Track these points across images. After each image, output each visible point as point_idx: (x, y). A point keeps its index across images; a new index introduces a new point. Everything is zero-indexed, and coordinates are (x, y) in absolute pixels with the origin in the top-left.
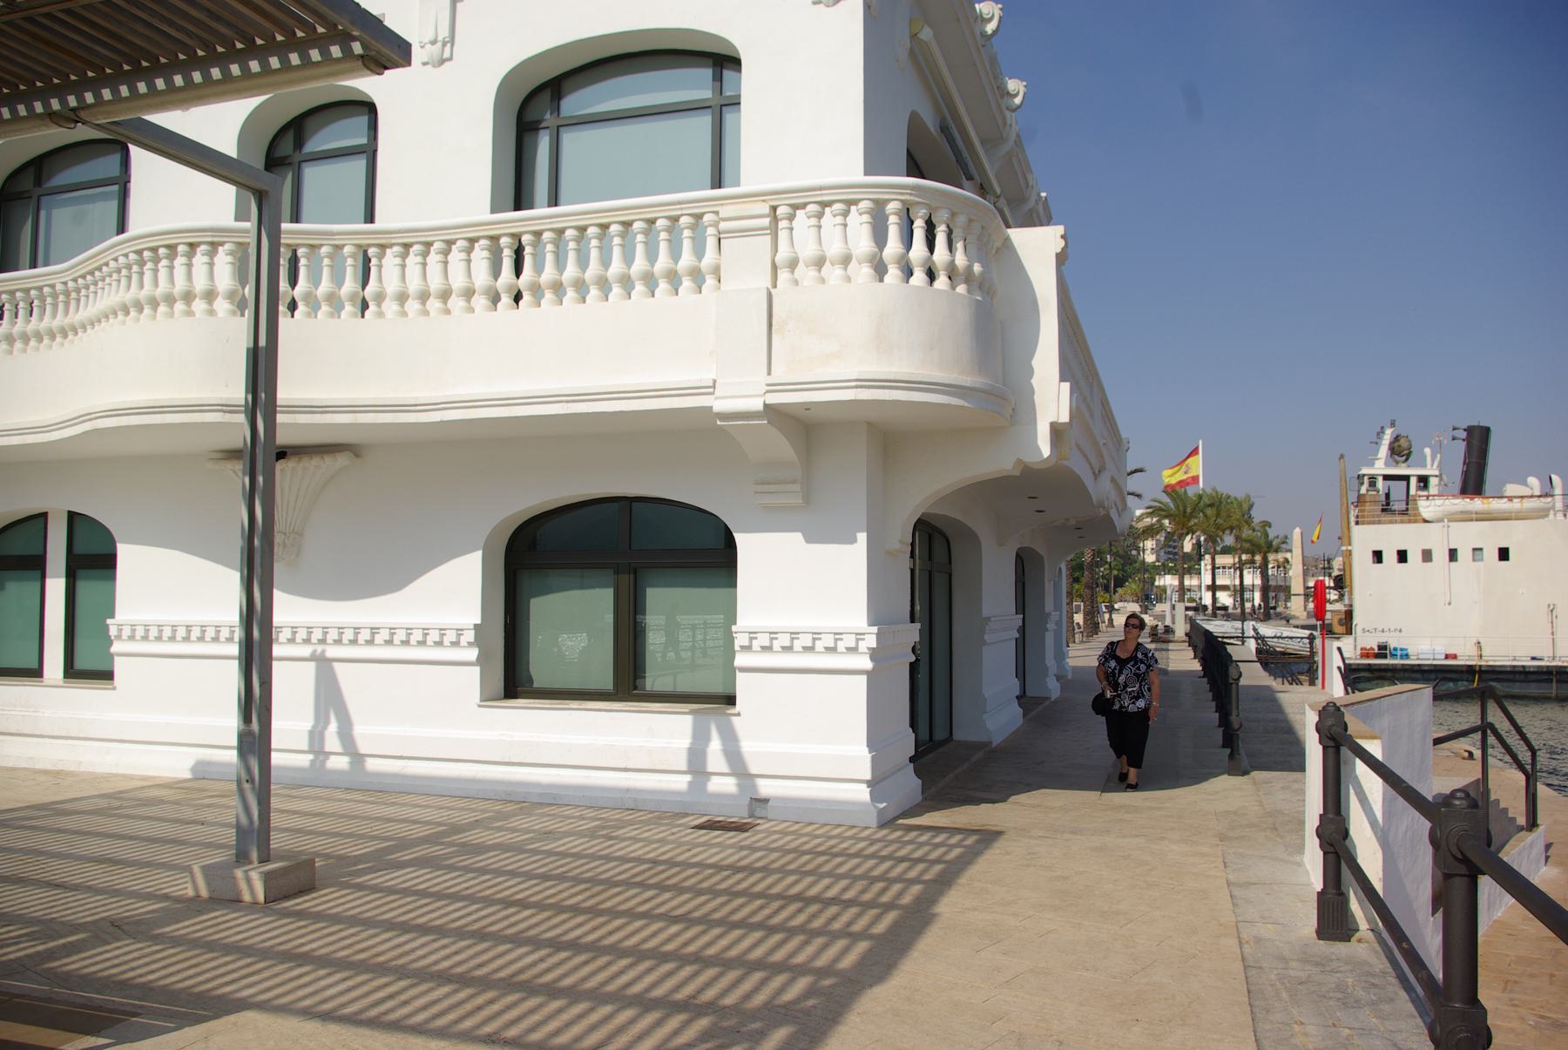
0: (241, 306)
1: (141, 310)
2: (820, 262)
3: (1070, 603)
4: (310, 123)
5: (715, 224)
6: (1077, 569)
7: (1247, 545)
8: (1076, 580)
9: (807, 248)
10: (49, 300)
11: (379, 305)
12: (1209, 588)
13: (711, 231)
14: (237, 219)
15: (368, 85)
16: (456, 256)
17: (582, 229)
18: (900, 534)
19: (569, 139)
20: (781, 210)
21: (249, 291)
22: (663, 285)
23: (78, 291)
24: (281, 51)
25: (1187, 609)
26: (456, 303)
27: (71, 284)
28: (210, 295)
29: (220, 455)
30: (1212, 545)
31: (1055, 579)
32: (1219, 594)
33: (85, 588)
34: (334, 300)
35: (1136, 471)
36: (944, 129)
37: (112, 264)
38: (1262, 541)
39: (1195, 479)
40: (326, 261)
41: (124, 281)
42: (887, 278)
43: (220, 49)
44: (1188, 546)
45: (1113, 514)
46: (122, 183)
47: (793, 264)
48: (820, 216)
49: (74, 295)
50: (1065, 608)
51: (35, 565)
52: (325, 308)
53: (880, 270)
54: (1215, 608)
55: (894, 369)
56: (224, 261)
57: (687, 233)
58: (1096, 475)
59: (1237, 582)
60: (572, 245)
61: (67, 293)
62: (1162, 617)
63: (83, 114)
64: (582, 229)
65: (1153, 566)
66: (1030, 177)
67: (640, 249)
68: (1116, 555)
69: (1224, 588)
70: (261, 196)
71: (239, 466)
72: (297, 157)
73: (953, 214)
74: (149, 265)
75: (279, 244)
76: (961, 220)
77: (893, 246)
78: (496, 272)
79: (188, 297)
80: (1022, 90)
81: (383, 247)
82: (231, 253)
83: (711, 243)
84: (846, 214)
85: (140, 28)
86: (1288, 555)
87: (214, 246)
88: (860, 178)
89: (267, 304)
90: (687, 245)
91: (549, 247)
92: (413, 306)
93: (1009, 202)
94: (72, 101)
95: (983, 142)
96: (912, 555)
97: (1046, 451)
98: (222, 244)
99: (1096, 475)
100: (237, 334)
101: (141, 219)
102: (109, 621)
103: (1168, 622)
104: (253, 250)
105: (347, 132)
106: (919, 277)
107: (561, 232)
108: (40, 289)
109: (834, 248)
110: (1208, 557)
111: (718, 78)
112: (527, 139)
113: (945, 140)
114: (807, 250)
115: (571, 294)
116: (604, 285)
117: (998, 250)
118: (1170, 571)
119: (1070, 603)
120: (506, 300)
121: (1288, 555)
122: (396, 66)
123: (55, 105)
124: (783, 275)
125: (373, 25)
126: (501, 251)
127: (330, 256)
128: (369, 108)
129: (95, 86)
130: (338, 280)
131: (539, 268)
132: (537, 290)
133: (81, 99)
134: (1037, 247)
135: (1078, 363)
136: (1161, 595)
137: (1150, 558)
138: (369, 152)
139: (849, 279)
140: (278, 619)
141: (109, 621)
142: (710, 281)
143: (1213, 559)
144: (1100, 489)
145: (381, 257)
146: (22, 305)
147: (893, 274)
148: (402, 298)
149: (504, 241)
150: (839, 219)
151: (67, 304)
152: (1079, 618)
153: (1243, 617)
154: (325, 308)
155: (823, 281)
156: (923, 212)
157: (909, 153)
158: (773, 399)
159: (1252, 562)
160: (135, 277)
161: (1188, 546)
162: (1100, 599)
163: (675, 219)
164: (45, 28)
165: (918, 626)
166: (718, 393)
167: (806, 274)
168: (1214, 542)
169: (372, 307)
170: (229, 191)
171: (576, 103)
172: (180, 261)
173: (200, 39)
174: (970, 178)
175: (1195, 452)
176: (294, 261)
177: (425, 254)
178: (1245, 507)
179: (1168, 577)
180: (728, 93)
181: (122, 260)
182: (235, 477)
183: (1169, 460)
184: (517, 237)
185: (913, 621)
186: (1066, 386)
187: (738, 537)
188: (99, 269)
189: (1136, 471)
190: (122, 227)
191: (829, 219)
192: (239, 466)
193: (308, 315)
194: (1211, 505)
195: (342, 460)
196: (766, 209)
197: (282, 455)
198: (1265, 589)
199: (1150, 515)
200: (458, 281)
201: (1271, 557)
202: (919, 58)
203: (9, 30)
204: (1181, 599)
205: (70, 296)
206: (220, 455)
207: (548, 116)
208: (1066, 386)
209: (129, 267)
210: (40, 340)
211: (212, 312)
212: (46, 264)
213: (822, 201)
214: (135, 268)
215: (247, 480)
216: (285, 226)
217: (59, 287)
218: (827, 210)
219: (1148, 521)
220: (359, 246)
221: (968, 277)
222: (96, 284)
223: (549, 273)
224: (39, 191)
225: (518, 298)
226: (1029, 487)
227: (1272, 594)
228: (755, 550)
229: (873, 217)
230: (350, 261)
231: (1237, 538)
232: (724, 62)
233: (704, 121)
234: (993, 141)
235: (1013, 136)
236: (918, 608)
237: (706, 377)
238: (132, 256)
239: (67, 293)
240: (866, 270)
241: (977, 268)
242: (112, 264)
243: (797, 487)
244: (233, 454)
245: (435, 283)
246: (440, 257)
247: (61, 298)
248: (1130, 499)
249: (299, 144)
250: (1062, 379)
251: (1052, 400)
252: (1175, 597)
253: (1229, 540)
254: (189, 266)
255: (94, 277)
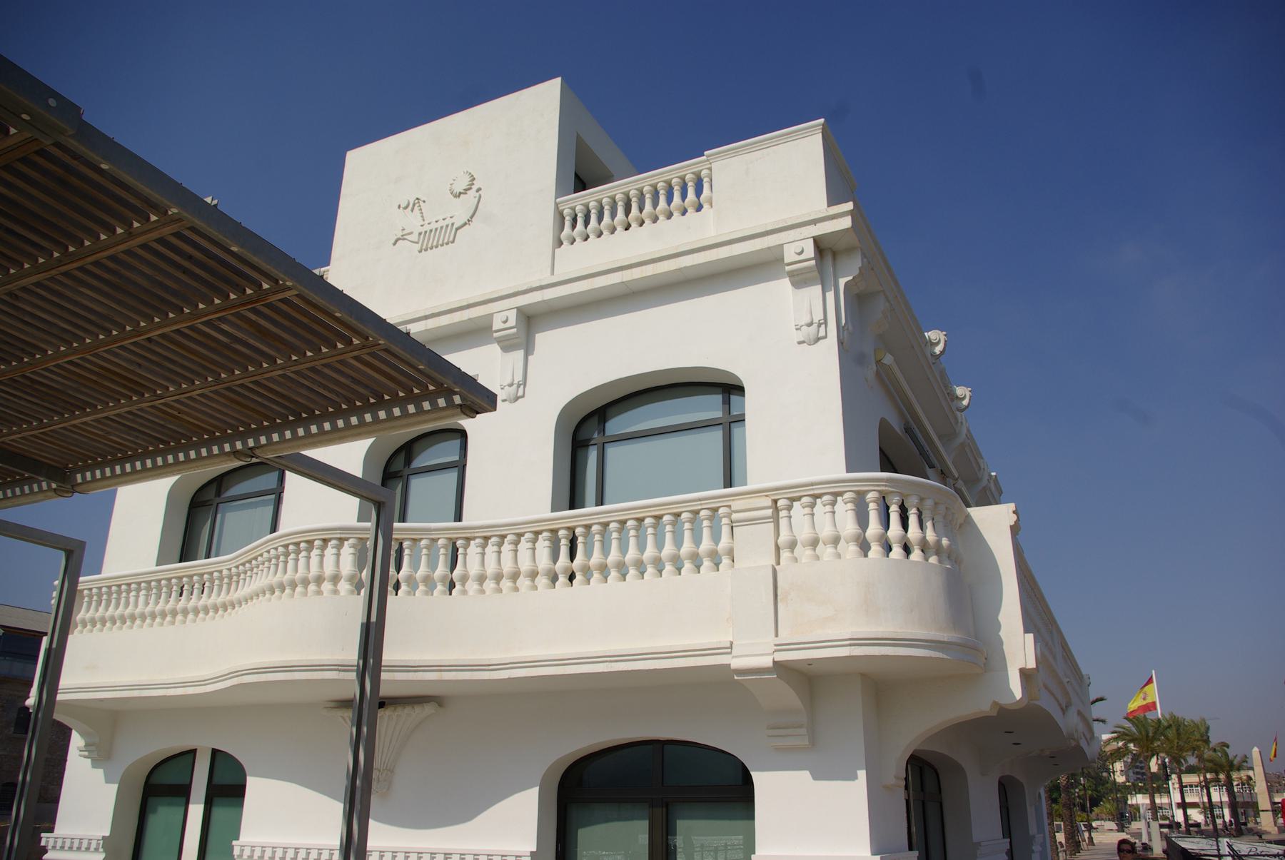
0: (358, 586)
1: (283, 590)
2: (814, 543)
3: (1051, 824)
4: (417, 446)
5: (728, 516)
6: (1054, 790)
7: (1209, 765)
8: (1055, 801)
9: (803, 532)
10: (217, 582)
11: (463, 585)
12: (1179, 805)
13: (725, 521)
14: (359, 521)
15: (466, 423)
16: (524, 545)
17: (623, 522)
18: (895, 770)
19: (612, 452)
20: (780, 503)
21: (365, 574)
22: (688, 565)
23: (238, 575)
24: (402, 403)
25: (1162, 826)
26: (524, 582)
27: (234, 570)
28: (335, 579)
29: (332, 704)
30: (1177, 765)
31: (1036, 801)
32: (1189, 811)
33: (219, 813)
34: (428, 580)
35: (1097, 700)
36: (908, 430)
37: (266, 555)
38: (1224, 760)
39: (1152, 706)
40: (425, 551)
41: (273, 567)
42: (871, 554)
43: (358, 404)
44: (1154, 766)
45: (1083, 744)
46: (278, 494)
47: (792, 545)
48: (813, 506)
49: (235, 578)
50: (1047, 828)
51: (182, 793)
52: (422, 587)
53: (864, 547)
54: (1188, 825)
55: (881, 629)
56: (348, 552)
57: (706, 523)
58: (1064, 711)
59: (1206, 799)
60: (615, 535)
61: (230, 577)
62: (1139, 835)
63: (257, 452)
64: (623, 522)
65: (1123, 786)
66: (980, 461)
67: (668, 537)
68: (1087, 776)
69: (1194, 805)
70: (379, 506)
71: (349, 714)
72: (406, 471)
73: (922, 500)
74: (292, 556)
75: (391, 539)
76: (929, 503)
77: (874, 527)
78: (555, 557)
79: (319, 580)
80: (943, 339)
81: (468, 539)
82: (353, 546)
83: (725, 530)
84: (833, 503)
85: (304, 392)
86: (1250, 773)
87: (342, 540)
88: (843, 474)
89: (379, 584)
90: (706, 533)
91: (597, 537)
92: (489, 585)
93: (965, 482)
94: (251, 443)
95: (940, 437)
96: (907, 787)
97: (1018, 694)
98: (347, 539)
99: (1064, 711)
100: (354, 609)
101: (290, 521)
102: (234, 843)
103: (1145, 839)
104: (370, 544)
105: (444, 452)
106: (897, 552)
107: (606, 525)
108: (211, 574)
109: (826, 531)
110: (1174, 776)
111: (727, 402)
112: (580, 453)
113: (910, 442)
114: (804, 533)
115: (614, 574)
116: (640, 567)
117: (961, 526)
118: (1140, 790)
119: (1051, 824)
120: (562, 579)
121: (1250, 773)
122: (486, 411)
123: (239, 445)
124: (785, 554)
125: (469, 383)
126: (559, 541)
127: (428, 547)
128: (462, 434)
129: (267, 432)
130: (433, 565)
131: (588, 554)
132: (587, 571)
133: (257, 441)
134: (994, 522)
135: (1038, 615)
136: (1135, 813)
137: (1120, 779)
138: (460, 467)
139: (839, 556)
140: (372, 843)
141: (234, 843)
142: (725, 561)
143: (1180, 779)
144: (1069, 723)
145: (466, 547)
146: (196, 586)
147: (875, 550)
148: (481, 579)
149: (562, 533)
150: (828, 508)
151: (229, 585)
152: (1060, 837)
153: (1215, 834)
154: (422, 587)
155: (818, 558)
156: (896, 499)
157: (880, 449)
158: (781, 657)
159: (1218, 780)
160: (281, 565)
161: (1154, 766)
162: (1078, 819)
163: (696, 513)
164: (239, 394)
165: (916, 853)
166: (735, 652)
167: (804, 553)
168: (1179, 763)
169: (458, 586)
170: (354, 502)
171: (616, 425)
172: (315, 552)
173: (344, 397)
174: (932, 466)
175: (1150, 681)
176: (400, 551)
177: (500, 544)
178: (1203, 730)
179: (1140, 796)
180: (734, 413)
181: (273, 552)
182: (344, 725)
183: (1131, 688)
184: (572, 530)
185: (911, 849)
186: (1030, 637)
187: (755, 775)
188: (256, 558)
189: (1097, 700)
190: (274, 528)
191: (820, 508)
192: (349, 714)
193: (409, 593)
194: (1170, 726)
195: (428, 709)
196: (768, 502)
197: (382, 705)
198: (1233, 806)
199: (1115, 739)
200: (525, 565)
201: (1235, 775)
202: (884, 378)
203: (216, 397)
204: (1155, 818)
205: (232, 579)
206: (332, 704)
207: (596, 435)
208: (1030, 637)
209: (277, 557)
210: (207, 613)
211: (336, 592)
212: (217, 556)
213: (814, 494)
214: (282, 558)
215: (354, 730)
216: (396, 525)
217: (225, 572)
218: (818, 501)
219: (1114, 745)
220: (450, 539)
221: (938, 550)
222: (252, 570)
223: (596, 558)
224: (218, 500)
225: (572, 577)
226: (1006, 722)
227: (1241, 810)
228: (772, 788)
229: (856, 505)
230: (442, 551)
231: (1200, 758)
232: (730, 389)
233: (717, 435)
234: (949, 435)
235: (964, 431)
236: (914, 829)
237: (724, 639)
238: (281, 549)
239: (230, 577)
240: (853, 548)
241: (945, 542)
242: (266, 555)
243: (803, 731)
244: (344, 704)
245: (507, 566)
246: (512, 547)
247: (226, 580)
248: (1096, 725)
249: (408, 461)
250: (1026, 631)
251: (1019, 649)
252: (1149, 814)
253: (1192, 761)
254: (322, 556)
255: (250, 565)
